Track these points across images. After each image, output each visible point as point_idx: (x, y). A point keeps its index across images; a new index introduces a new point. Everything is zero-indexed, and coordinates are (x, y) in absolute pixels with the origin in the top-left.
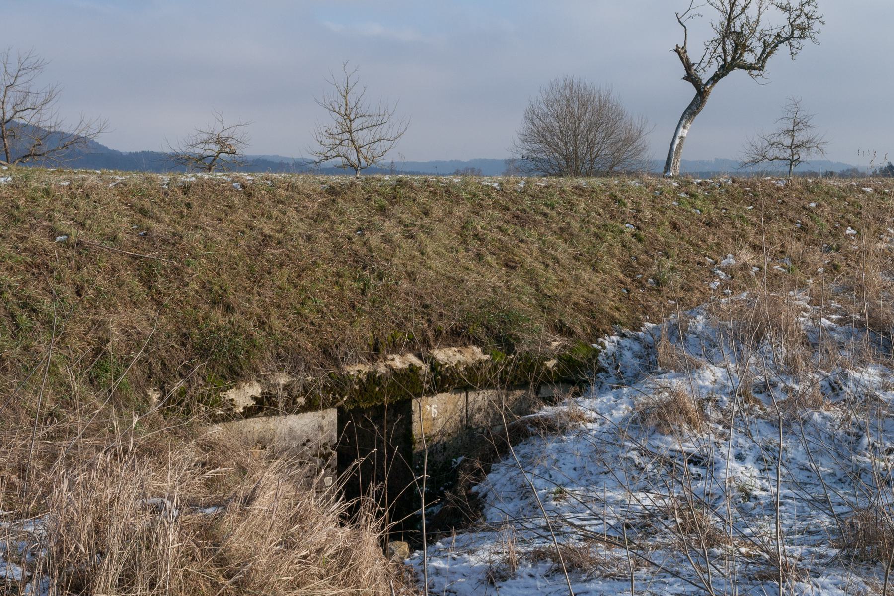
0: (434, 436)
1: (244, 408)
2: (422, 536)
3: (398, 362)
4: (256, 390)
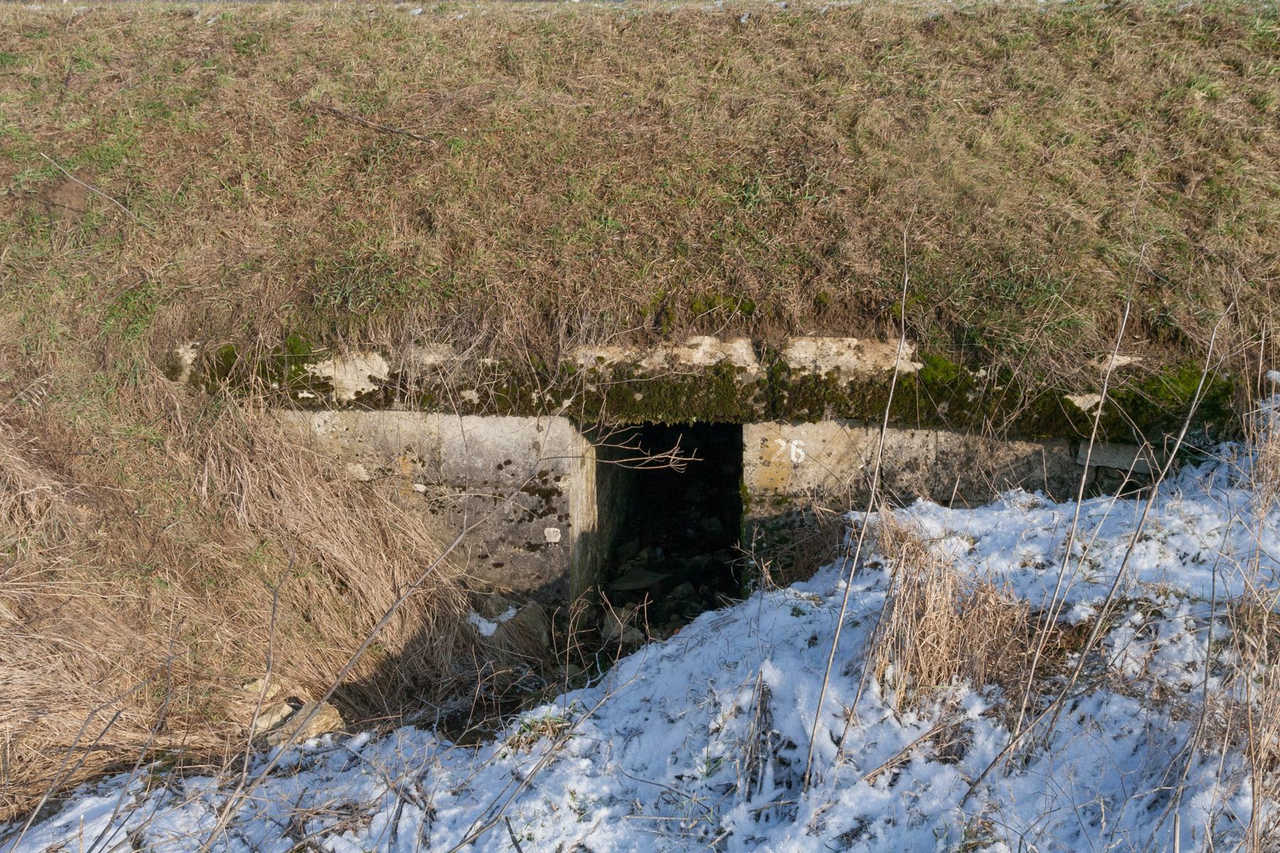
0: (796, 496)
1: (358, 393)
2: (1079, 481)
3: (701, 351)
4: (379, 367)
